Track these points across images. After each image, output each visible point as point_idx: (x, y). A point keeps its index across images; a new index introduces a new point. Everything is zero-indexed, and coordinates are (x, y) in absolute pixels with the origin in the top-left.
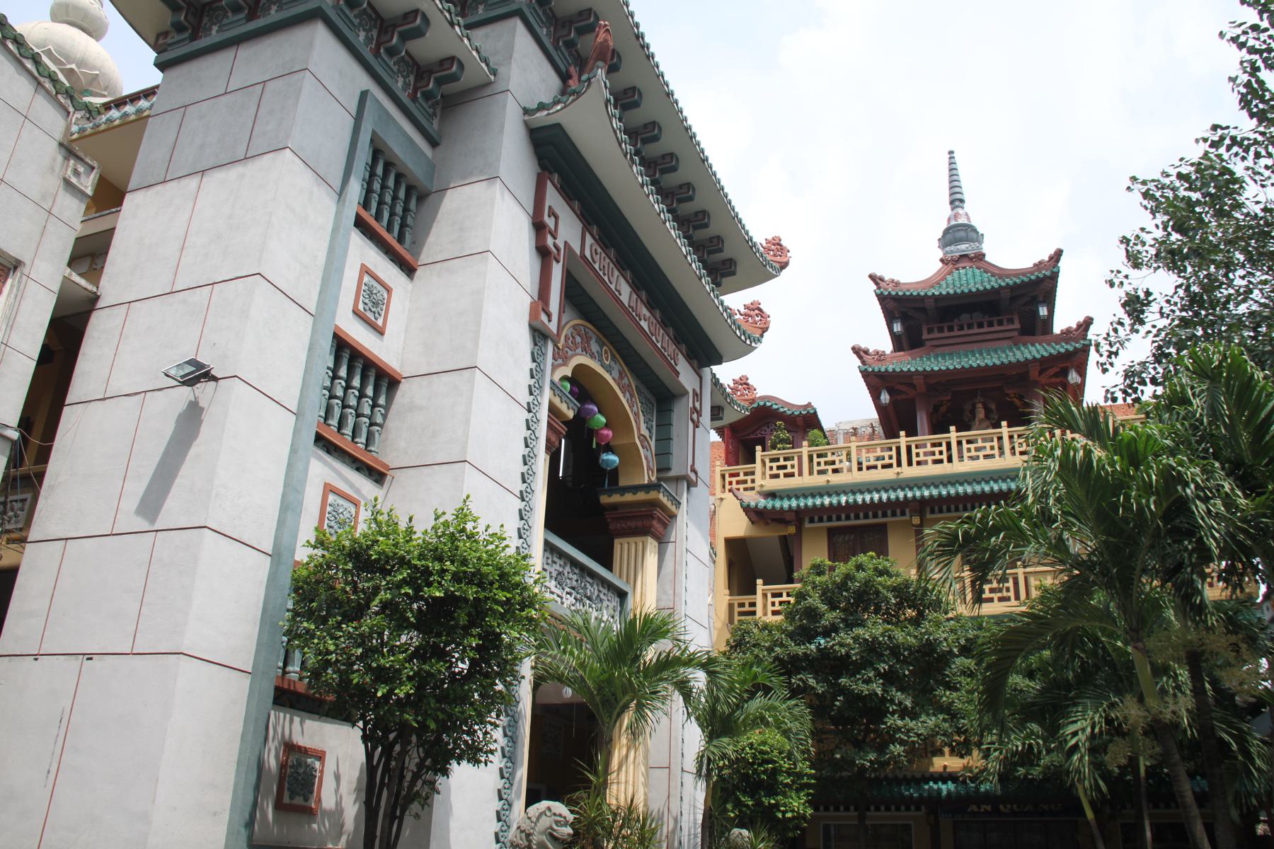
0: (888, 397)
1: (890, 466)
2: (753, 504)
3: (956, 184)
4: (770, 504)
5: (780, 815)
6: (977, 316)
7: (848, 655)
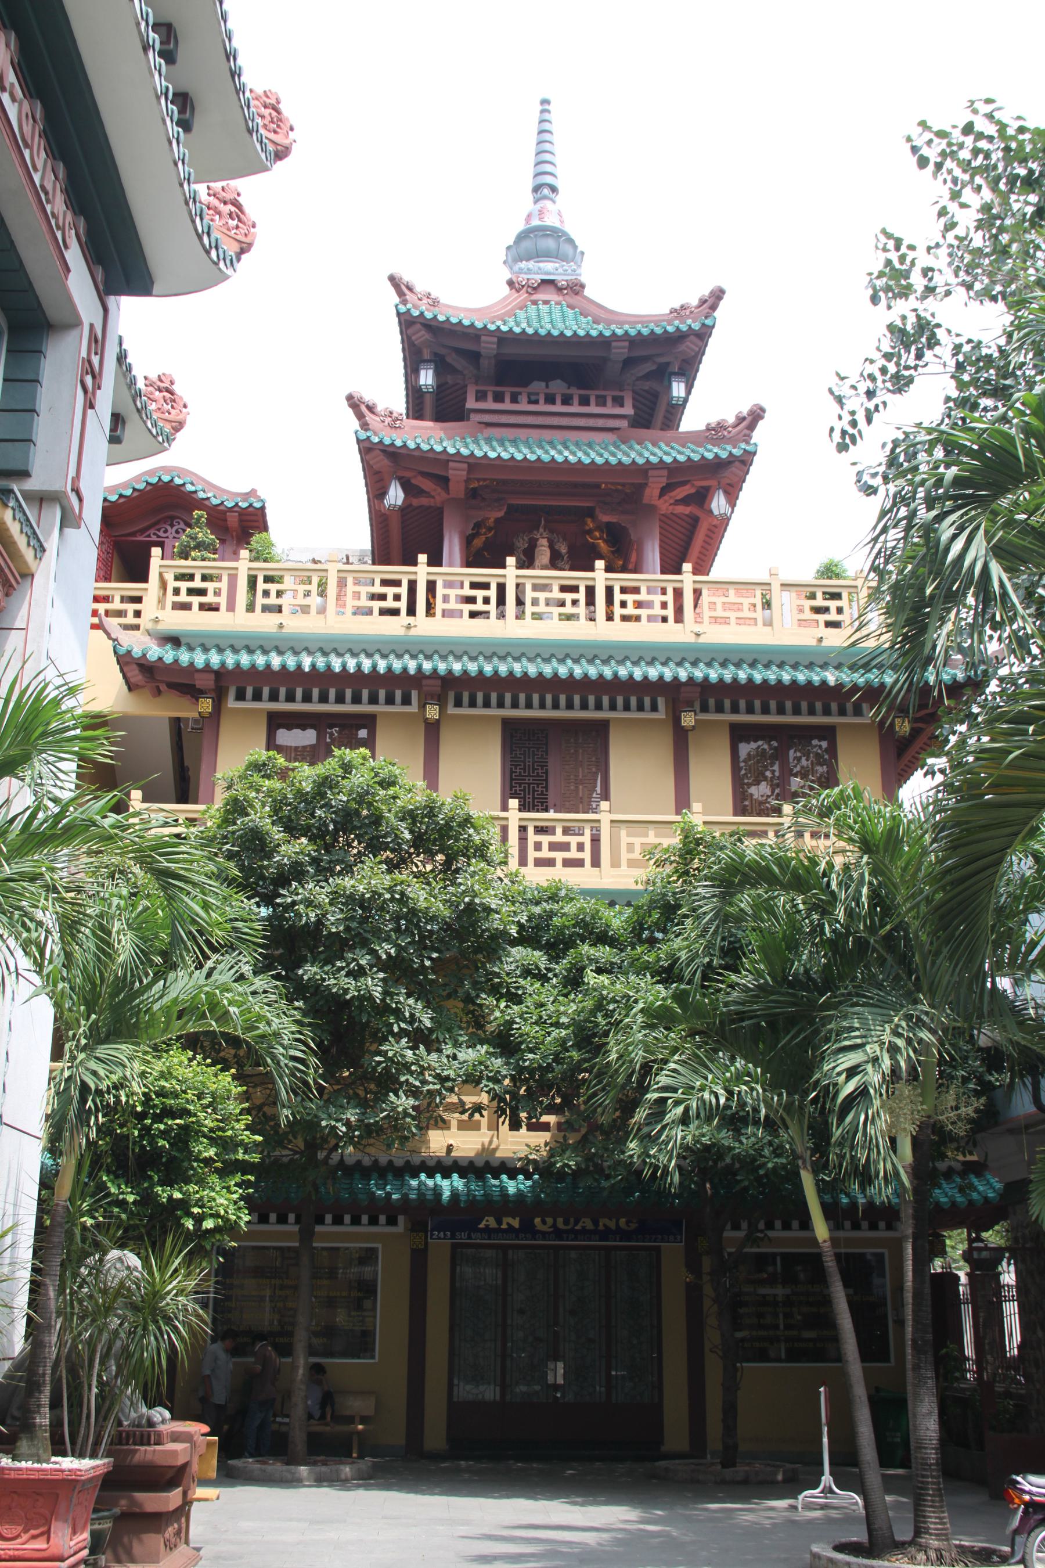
0: (401, 495)
1: (395, 612)
2: (137, 652)
3: (547, 157)
4: (169, 655)
5: (189, 1224)
6: (558, 387)
7: (320, 922)
